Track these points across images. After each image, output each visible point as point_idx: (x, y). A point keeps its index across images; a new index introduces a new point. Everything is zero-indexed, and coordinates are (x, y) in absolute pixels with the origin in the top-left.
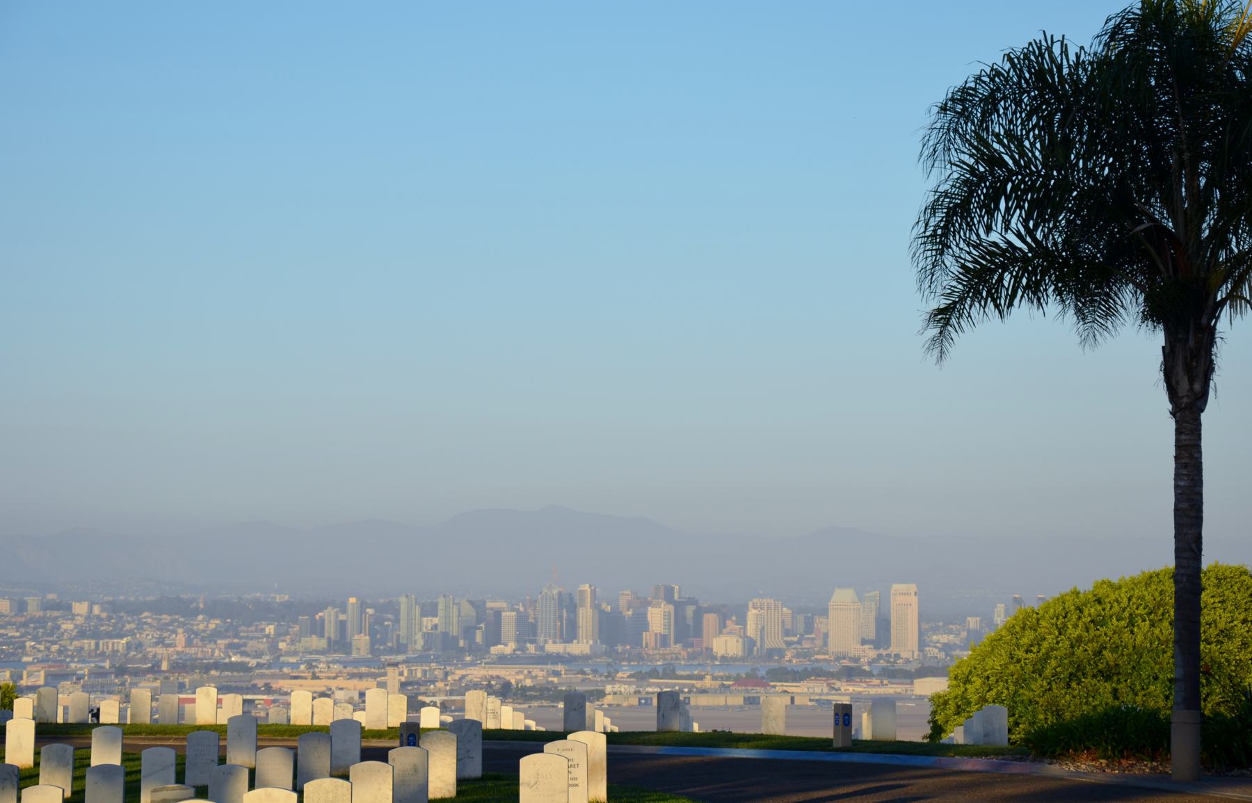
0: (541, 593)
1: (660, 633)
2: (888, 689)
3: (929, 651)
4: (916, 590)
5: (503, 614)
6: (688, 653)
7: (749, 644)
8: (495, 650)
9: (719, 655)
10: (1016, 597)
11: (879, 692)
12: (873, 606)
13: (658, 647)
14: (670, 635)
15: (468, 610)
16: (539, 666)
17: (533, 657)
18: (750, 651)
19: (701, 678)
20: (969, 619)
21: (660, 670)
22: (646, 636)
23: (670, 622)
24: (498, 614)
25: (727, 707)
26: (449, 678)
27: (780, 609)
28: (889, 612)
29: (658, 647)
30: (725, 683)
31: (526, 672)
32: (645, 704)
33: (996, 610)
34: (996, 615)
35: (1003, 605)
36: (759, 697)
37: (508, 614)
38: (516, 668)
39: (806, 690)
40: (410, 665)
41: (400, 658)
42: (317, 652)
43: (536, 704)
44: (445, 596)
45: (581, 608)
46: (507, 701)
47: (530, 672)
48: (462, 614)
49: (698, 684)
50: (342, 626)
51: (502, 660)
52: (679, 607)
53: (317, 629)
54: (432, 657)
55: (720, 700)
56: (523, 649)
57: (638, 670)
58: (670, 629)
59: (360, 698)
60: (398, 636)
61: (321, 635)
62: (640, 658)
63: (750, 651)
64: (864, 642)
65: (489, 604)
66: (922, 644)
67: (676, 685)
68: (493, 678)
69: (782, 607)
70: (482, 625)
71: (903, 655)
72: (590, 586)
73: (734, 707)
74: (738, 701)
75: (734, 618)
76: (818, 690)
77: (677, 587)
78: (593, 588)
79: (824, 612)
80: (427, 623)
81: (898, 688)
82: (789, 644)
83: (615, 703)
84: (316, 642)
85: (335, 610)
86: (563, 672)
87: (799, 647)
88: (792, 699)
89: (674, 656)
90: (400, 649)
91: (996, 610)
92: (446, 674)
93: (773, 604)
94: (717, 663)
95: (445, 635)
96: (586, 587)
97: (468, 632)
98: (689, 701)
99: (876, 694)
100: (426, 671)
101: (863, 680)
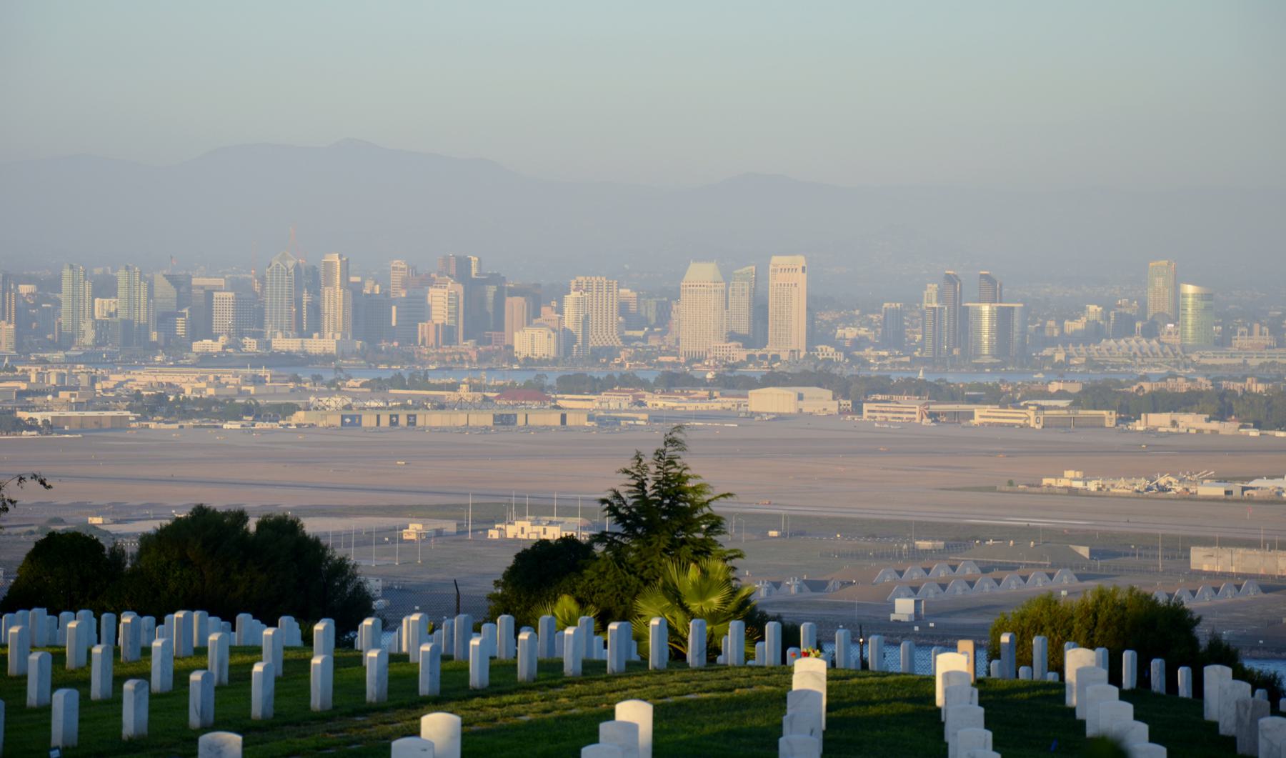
0: (270, 265)
2: (712, 404)
3: (822, 350)
4: (804, 265)
5: (216, 294)
6: (478, 352)
7: (566, 339)
8: (198, 346)
10: (948, 274)
11: (700, 408)
12: (747, 288)
13: (440, 344)
15: (164, 289)
16: (233, 370)
17: (253, 357)
18: (568, 351)
19: (454, 387)
21: (407, 377)
22: (423, 327)
24: (209, 294)
25: (467, 427)
26: (98, 386)
27: (615, 290)
31: (211, 378)
32: (351, 424)
33: (925, 292)
35: (936, 286)
36: (515, 415)
37: (223, 294)
38: (197, 373)
40: (48, 366)
41: (59, 355)
44: (127, 268)
46: (155, 419)
47: (217, 378)
48: (157, 294)
49: (449, 396)
51: (206, 360)
52: (473, 287)
54: (104, 356)
55: (460, 419)
56: (237, 346)
60: (60, 324)
62: (409, 358)
63: (568, 351)
64: (732, 337)
65: (195, 281)
66: (815, 335)
69: (619, 287)
70: (186, 311)
72: (340, 257)
73: (547, 429)
74: (486, 419)
76: (613, 405)
77: (474, 259)
78: (344, 259)
79: (675, 295)
80: (110, 305)
82: (627, 341)
83: (309, 422)
87: (641, 344)
88: (563, 418)
89: (457, 357)
90: (65, 342)
91: (925, 292)
92: (94, 380)
94: (516, 367)
95: (127, 324)
96: (334, 258)
97: (165, 320)
98: (415, 419)
99: (696, 411)
100: (64, 374)
101: (685, 392)
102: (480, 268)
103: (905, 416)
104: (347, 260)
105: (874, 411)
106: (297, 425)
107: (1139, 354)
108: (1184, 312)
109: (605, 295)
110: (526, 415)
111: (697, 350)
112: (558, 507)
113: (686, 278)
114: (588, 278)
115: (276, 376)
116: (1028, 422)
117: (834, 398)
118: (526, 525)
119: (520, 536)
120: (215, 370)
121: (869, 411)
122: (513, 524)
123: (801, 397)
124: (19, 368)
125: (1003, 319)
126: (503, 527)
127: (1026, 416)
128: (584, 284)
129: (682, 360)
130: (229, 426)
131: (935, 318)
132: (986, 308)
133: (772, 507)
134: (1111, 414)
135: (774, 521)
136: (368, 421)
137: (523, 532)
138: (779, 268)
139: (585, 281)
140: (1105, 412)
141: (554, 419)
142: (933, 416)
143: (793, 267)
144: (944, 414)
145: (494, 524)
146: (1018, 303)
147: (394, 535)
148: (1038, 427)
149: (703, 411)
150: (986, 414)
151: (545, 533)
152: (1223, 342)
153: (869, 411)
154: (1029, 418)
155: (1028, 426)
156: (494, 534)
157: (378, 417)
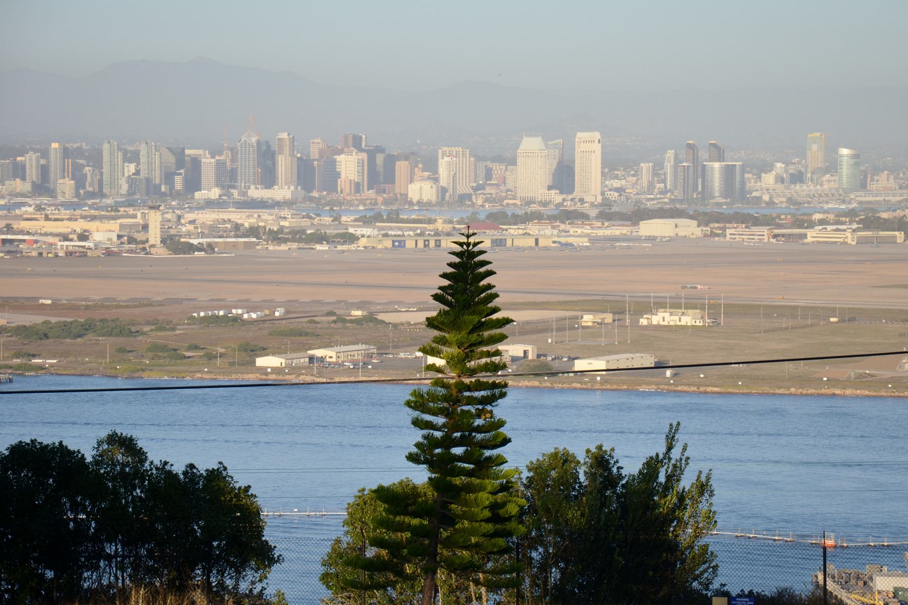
0: (240, 141)
1: (354, 180)
9: (415, 201)
11: (606, 234)
15: (171, 159)
16: (267, 211)
20: (642, 165)
23: (363, 169)
28: (574, 161)
29: (353, 193)
31: (256, 215)
34: (666, 161)
35: (673, 151)
36: (505, 240)
38: (246, 212)
39: (537, 232)
42: (23, 195)
43: (294, 246)
47: (259, 216)
50: (44, 171)
52: (372, 154)
53: (19, 172)
54: (139, 201)
56: (229, 195)
57: (364, 214)
58: (363, 175)
59: (118, 239)
61: (23, 179)
65: (187, 152)
67: (418, 228)
68: (225, 221)
70: (182, 171)
71: (587, 199)
72: (289, 135)
73: (523, 249)
75: (420, 166)
77: (364, 136)
78: (291, 136)
79: (513, 162)
81: (623, 229)
84: (19, 185)
85: (37, 154)
86: (289, 216)
88: (537, 241)
93: (461, 153)
95: (148, 180)
96: (284, 135)
98: (440, 243)
99: (603, 236)
103: (756, 237)
104: (293, 137)
105: (734, 234)
106: (364, 247)
107: (816, 195)
108: (841, 167)
109: (461, 160)
110: (513, 240)
111: (522, 196)
112: (724, 304)
114: (450, 148)
115: (294, 215)
116: (846, 240)
117: (698, 226)
118: (667, 315)
119: (662, 323)
120: (259, 210)
121: (730, 234)
122: (657, 314)
123: (676, 226)
124: (122, 209)
125: (729, 172)
126: (650, 317)
127: (845, 236)
128: (448, 152)
130: (318, 247)
131: (684, 173)
132: (717, 165)
133: (784, 300)
134: (901, 234)
135: (832, 312)
136: (410, 244)
137: (664, 320)
138: (582, 140)
139: (448, 151)
140: (897, 233)
141: (531, 242)
142: (775, 236)
143: (592, 139)
144: (783, 236)
145: (643, 315)
146: (739, 162)
147: (572, 325)
148: (854, 243)
149: (607, 236)
150: (816, 235)
151: (680, 321)
152: (863, 186)
153: (730, 234)
154: (847, 238)
155: (846, 243)
156: (643, 322)
157: (416, 241)
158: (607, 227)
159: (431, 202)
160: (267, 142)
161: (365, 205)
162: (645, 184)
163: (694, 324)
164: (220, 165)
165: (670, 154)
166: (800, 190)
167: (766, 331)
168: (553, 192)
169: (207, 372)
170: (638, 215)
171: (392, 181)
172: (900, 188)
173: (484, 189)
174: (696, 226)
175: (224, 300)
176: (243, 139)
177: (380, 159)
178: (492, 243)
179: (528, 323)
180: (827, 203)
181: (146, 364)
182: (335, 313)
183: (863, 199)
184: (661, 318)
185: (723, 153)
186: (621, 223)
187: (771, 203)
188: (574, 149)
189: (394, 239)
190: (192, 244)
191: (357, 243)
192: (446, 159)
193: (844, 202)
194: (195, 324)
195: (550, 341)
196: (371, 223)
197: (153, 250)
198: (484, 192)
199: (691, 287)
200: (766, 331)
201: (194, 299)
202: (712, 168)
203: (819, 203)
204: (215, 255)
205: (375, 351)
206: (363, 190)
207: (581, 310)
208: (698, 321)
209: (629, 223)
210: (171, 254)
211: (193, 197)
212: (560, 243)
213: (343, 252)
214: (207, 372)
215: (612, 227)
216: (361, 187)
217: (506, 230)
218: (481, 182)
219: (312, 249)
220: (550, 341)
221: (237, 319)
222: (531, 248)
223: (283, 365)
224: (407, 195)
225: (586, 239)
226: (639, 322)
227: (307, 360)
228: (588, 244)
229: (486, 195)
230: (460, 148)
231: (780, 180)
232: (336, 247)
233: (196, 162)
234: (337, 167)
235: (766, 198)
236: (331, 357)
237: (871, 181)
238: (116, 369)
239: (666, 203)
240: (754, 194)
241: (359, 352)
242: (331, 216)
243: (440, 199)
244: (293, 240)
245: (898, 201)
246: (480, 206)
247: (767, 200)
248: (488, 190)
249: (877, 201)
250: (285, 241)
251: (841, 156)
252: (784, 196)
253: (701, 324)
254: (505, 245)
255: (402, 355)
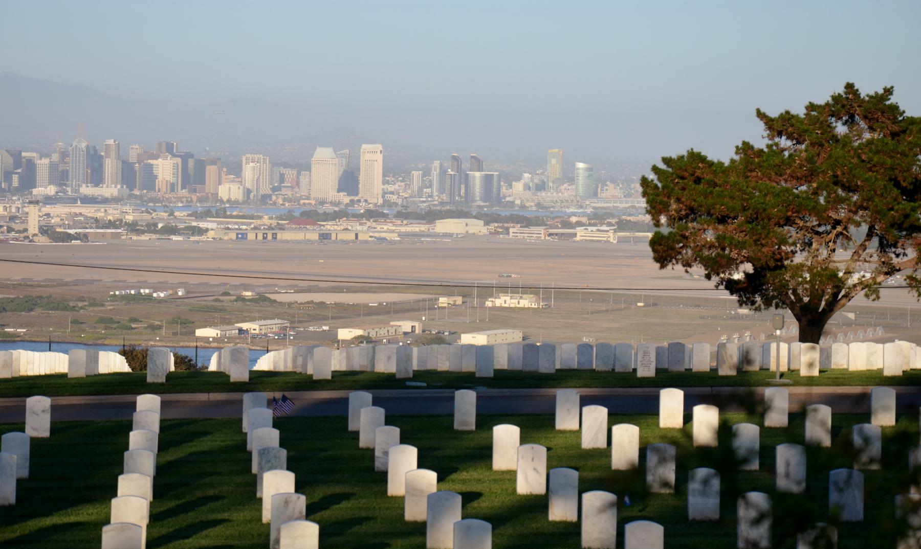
9: (225, 199)
14: (178, 182)
15: (10, 160)
18: (248, 197)
23: (178, 172)
28: (359, 169)
29: (168, 192)
30: (280, 222)
31: (103, 210)
32: (242, 238)
34: (433, 170)
36: (331, 234)
43: (154, 237)
45: (107, 160)
47: (106, 211)
52: (185, 157)
56: (65, 192)
58: (177, 177)
65: (24, 154)
70: (19, 171)
72: (115, 141)
75: (225, 169)
77: (175, 144)
78: (117, 143)
79: (308, 168)
86: (131, 211)
88: (357, 235)
96: (111, 142)
102: (177, 149)
103: (535, 235)
105: (516, 233)
113: (315, 156)
118: (508, 299)
119: (504, 305)
121: (513, 233)
123: (467, 225)
125: (488, 180)
126: (494, 300)
129: (313, 202)
130: (174, 238)
132: (477, 174)
136: (251, 236)
137: (505, 303)
141: (351, 237)
142: (550, 235)
144: (556, 234)
148: (615, 242)
151: (519, 303)
153: (513, 233)
154: (609, 237)
155: (609, 242)
156: (489, 304)
157: (256, 234)
158: (406, 225)
159: (238, 201)
160: (95, 147)
161: (182, 202)
162: (416, 189)
163: (530, 306)
164: (53, 167)
165: (436, 164)
166: (546, 196)
167: (592, 313)
168: (342, 194)
169: (159, 341)
170: (431, 216)
171: (203, 182)
172: (625, 196)
173: (281, 191)
174: (483, 225)
175: (125, 281)
176: (74, 144)
177: (191, 164)
178: (319, 236)
179: (394, 303)
180: (568, 207)
181: (101, 334)
182: (229, 293)
183: (597, 205)
184: (504, 301)
185: (461, 165)
186: (418, 221)
187: (523, 207)
188: (359, 158)
189: (238, 232)
190: (70, 234)
191: (206, 235)
192: (252, 164)
193: (581, 207)
194: (116, 301)
195: (424, 318)
196: (202, 218)
197: (35, 239)
198: (281, 193)
199: (507, 276)
200: (592, 313)
201: (100, 281)
202: (474, 177)
203: (561, 207)
204: (89, 243)
205: (288, 325)
206: (177, 190)
207: (436, 294)
208: (533, 304)
209: (425, 222)
210: (51, 242)
211: (31, 193)
212: (375, 237)
213: (198, 242)
214: (159, 341)
215: (412, 225)
216: (176, 187)
217: (324, 226)
218: (276, 184)
219: (169, 239)
220: (424, 318)
221: (149, 297)
222: (353, 241)
223: (219, 336)
224: (217, 194)
225: (396, 235)
226: (485, 304)
227: (237, 331)
228: (399, 239)
229: (283, 195)
230: (261, 156)
231: (527, 187)
232: (189, 238)
233: (31, 166)
234: (154, 169)
235: (518, 202)
236: (254, 330)
237: (601, 190)
238: (81, 337)
239: (435, 205)
240: (508, 199)
241: (277, 326)
242: (165, 212)
243: (246, 197)
244: (149, 231)
245: (624, 208)
246: (281, 204)
247: (519, 203)
248: (284, 191)
249: (608, 207)
250: (143, 232)
251: (578, 169)
252: (533, 201)
253: (536, 307)
254: (330, 239)
255: (311, 329)
